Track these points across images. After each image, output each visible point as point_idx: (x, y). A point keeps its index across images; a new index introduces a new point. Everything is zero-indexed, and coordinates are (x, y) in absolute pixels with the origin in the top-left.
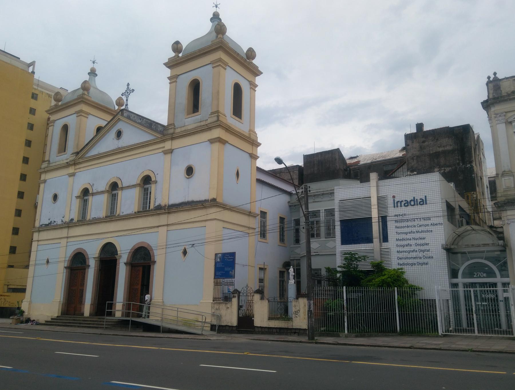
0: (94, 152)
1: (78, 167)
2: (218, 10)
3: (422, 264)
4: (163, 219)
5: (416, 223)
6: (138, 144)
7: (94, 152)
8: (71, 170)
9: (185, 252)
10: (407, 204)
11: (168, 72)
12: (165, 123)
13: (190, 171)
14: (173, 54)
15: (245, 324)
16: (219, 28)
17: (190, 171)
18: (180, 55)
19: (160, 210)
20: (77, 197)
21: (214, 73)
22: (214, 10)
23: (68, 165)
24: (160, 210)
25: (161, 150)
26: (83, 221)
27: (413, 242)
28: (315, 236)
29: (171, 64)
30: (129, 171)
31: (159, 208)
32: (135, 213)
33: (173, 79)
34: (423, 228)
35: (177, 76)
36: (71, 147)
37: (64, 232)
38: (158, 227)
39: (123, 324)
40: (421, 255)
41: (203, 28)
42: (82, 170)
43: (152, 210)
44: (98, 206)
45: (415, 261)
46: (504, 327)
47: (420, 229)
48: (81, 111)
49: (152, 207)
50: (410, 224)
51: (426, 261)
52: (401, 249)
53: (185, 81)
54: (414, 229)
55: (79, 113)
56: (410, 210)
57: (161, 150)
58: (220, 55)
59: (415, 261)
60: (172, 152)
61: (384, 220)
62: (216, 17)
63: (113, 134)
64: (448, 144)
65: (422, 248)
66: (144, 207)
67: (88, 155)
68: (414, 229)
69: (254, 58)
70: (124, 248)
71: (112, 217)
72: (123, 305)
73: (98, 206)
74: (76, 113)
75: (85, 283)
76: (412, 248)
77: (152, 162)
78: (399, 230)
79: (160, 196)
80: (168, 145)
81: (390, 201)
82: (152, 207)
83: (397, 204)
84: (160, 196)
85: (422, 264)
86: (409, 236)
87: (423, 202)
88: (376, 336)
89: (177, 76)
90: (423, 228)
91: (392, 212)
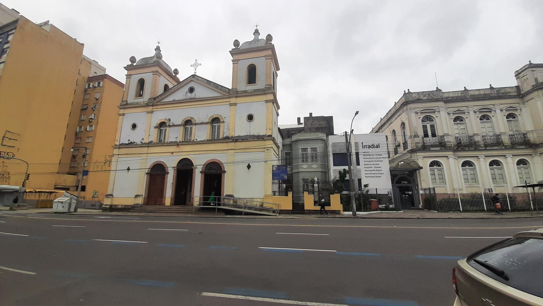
1: (155, 107)
2: (159, 45)
3: (378, 177)
4: (231, 145)
5: (374, 157)
6: (205, 98)
8: (150, 108)
10: (369, 147)
11: (126, 72)
12: (231, 88)
13: (134, 126)
14: (130, 63)
15: (298, 208)
16: (159, 56)
17: (134, 126)
18: (135, 64)
19: (227, 139)
20: (155, 127)
21: (256, 64)
22: (158, 45)
23: (147, 105)
24: (227, 139)
26: (161, 143)
27: (373, 166)
28: (310, 159)
29: (127, 68)
30: (177, 115)
31: (227, 138)
34: (378, 159)
35: (131, 75)
36: (147, 95)
37: (145, 150)
39: (201, 210)
40: (377, 172)
41: (152, 53)
43: (221, 139)
44: (174, 134)
45: (374, 175)
47: (376, 160)
48: (157, 71)
49: (221, 137)
50: (371, 157)
51: (380, 175)
52: (367, 169)
54: (373, 160)
55: (155, 73)
56: (371, 150)
57: (228, 103)
58: (156, 68)
59: (374, 175)
61: (357, 154)
62: (158, 49)
64: (324, 124)
65: (378, 169)
66: (160, 141)
68: (373, 160)
69: (178, 74)
71: (187, 141)
72: (200, 198)
73: (174, 134)
74: (152, 72)
76: (372, 169)
77: (220, 109)
78: (366, 160)
79: (225, 131)
80: (233, 100)
81: (360, 146)
82: (221, 137)
83: (364, 147)
84: (225, 131)
85: (378, 177)
86: (371, 163)
87: (378, 146)
89: (131, 75)
90: (378, 159)
91: (361, 150)
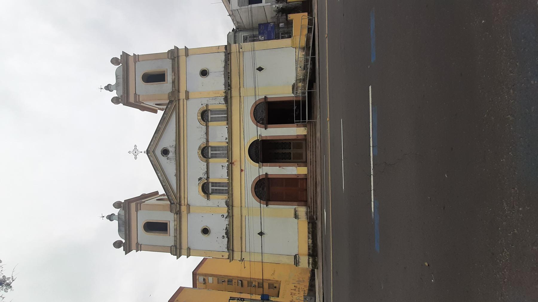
0: (174, 186)
1: (183, 202)
7: (174, 186)
9: (260, 69)
25: (185, 101)
29: (127, 250)
32: (227, 124)
33: (139, 248)
38: (240, 96)
42: (186, 197)
46: (304, 160)
53: (144, 236)
60: (190, 249)
63: (163, 159)
67: (174, 112)
70: (253, 171)
73: (219, 172)
74: (137, 211)
75: (278, 100)
77: (191, 111)
80: (182, 95)
88: (308, 228)
